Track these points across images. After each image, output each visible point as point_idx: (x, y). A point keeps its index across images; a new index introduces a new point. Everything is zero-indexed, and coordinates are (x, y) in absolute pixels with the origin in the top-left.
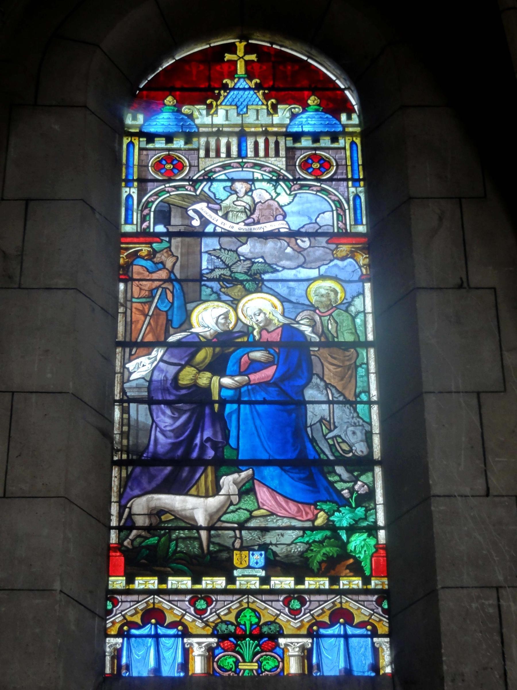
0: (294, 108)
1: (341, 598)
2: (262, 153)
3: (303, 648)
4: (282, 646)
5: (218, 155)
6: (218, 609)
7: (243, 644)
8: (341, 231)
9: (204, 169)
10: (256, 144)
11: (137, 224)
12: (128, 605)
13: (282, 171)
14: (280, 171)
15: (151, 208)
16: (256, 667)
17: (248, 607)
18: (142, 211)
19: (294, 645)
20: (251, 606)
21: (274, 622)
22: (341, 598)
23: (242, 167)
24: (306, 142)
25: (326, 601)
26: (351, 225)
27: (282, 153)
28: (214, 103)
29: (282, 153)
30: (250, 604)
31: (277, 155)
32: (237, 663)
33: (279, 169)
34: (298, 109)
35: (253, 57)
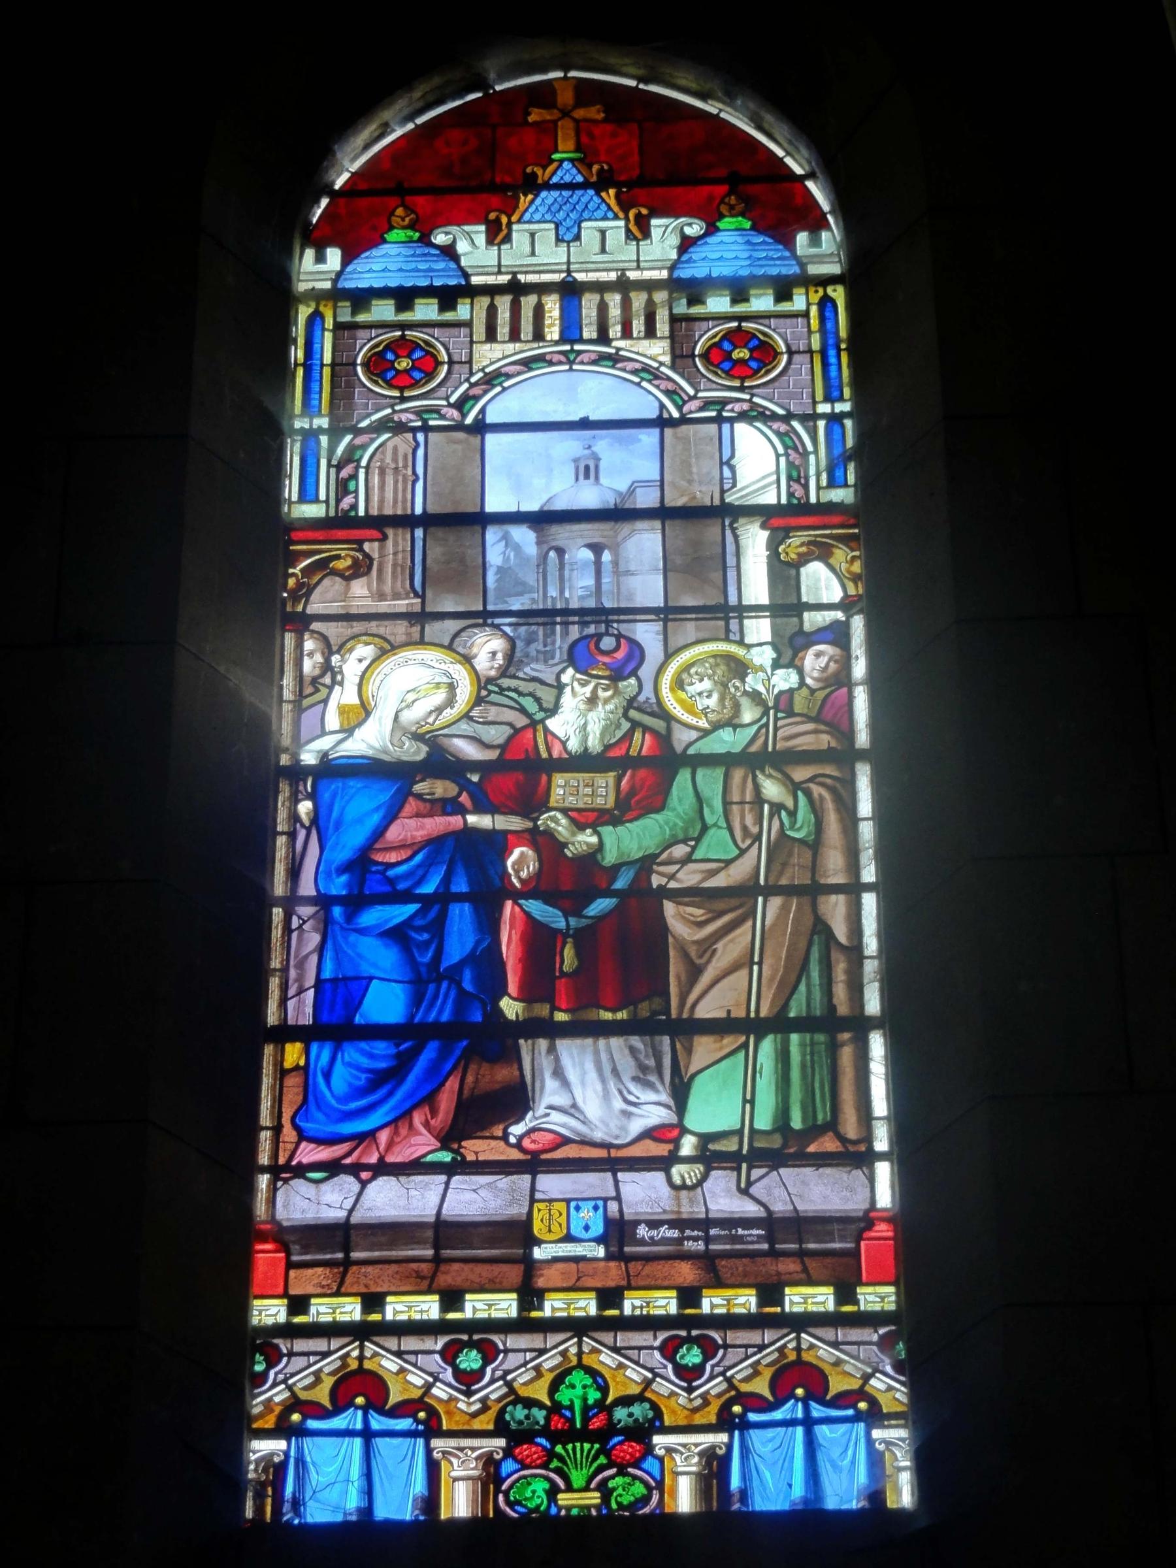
0: (690, 225)
1: (362, 1348)
2: (615, 331)
3: (709, 1455)
4: (660, 1452)
5: (515, 336)
6: (293, 1375)
7: (567, 1451)
8: (795, 502)
9: (483, 370)
10: (603, 308)
11: (327, 502)
12: (517, 1359)
13: (663, 369)
14: (657, 369)
15: (359, 461)
16: (598, 1501)
17: (580, 1365)
18: (339, 467)
19: (689, 1450)
20: (586, 1360)
21: (640, 1398)
22: (362, 1348)
23: (571, 363)
24: (718, 303)
25: (325, 1355)
26: (819, 488)
27: (663, 328)
28: (504, 220)
29: (663, 328)
30: (584, 1356)
31: (650, 332)
32: (553, 1492)
33: (655, 365)
34: (695, 228)
35: (595, 113)
